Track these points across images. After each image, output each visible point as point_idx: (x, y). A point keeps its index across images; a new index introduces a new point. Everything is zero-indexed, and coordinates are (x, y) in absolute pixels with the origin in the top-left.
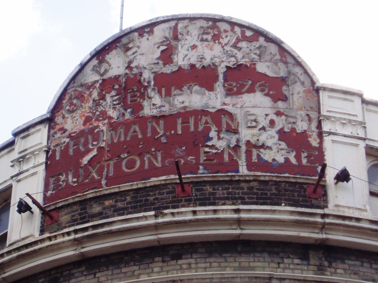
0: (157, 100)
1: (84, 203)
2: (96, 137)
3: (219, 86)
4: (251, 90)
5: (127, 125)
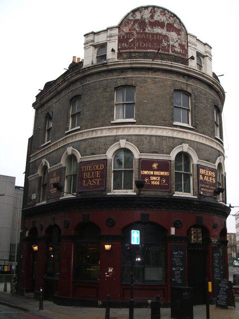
0: (149, 28)
1: (130, 53)
2: (133, 35)
3: (165, 28)
4: (172, 31)
5: (141, 34)
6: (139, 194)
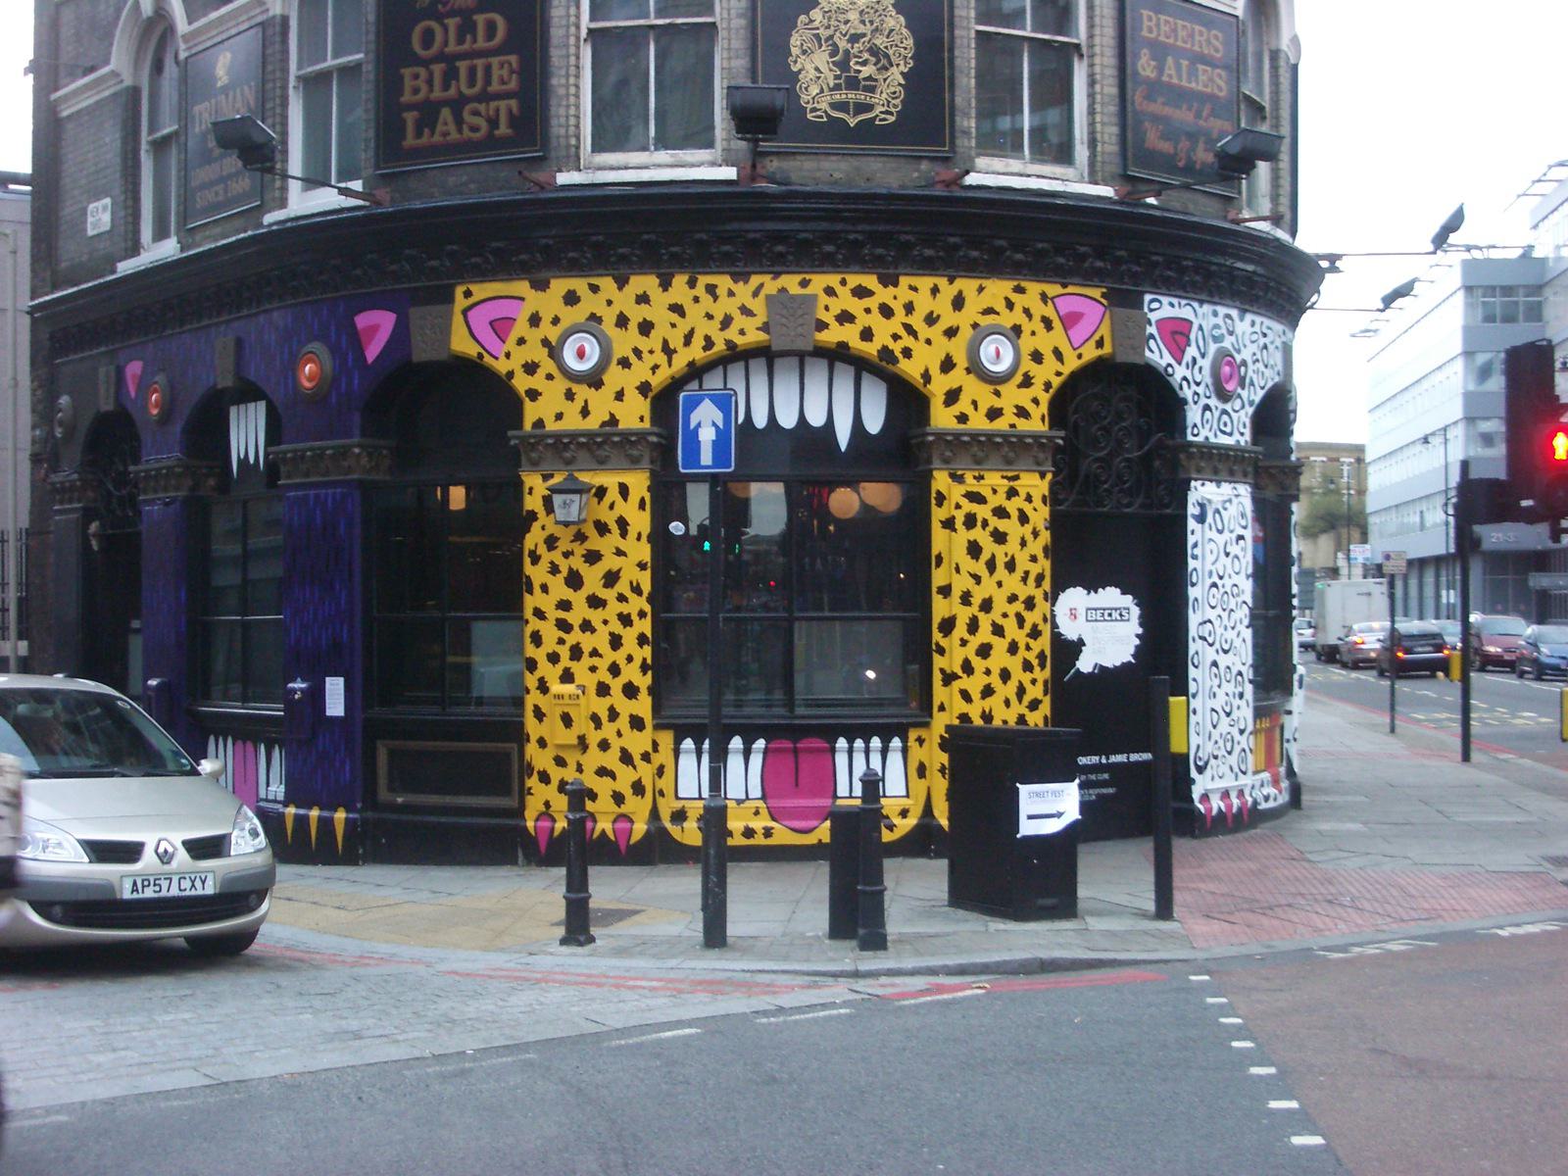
6: (751, 172)
